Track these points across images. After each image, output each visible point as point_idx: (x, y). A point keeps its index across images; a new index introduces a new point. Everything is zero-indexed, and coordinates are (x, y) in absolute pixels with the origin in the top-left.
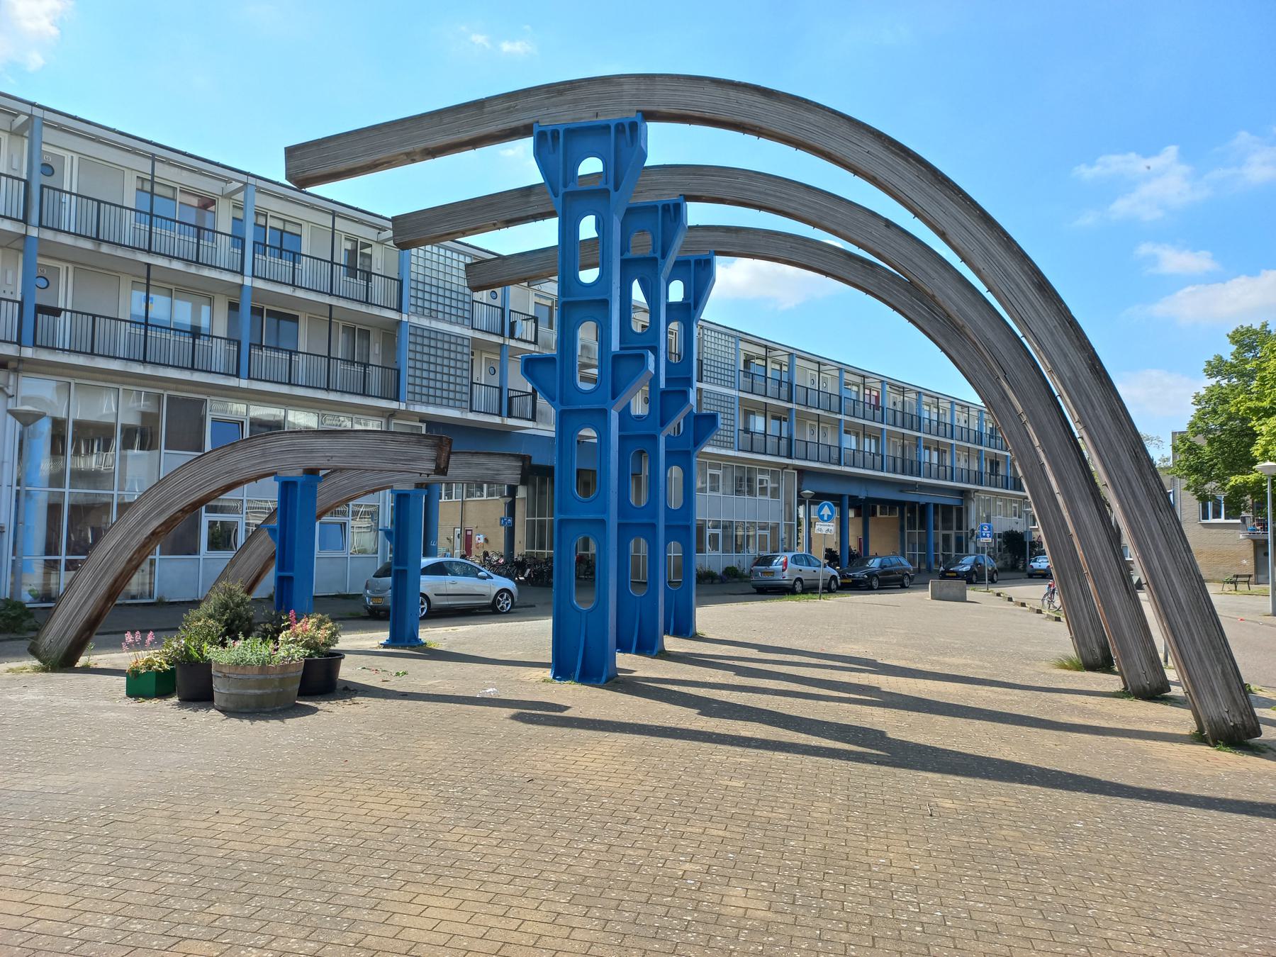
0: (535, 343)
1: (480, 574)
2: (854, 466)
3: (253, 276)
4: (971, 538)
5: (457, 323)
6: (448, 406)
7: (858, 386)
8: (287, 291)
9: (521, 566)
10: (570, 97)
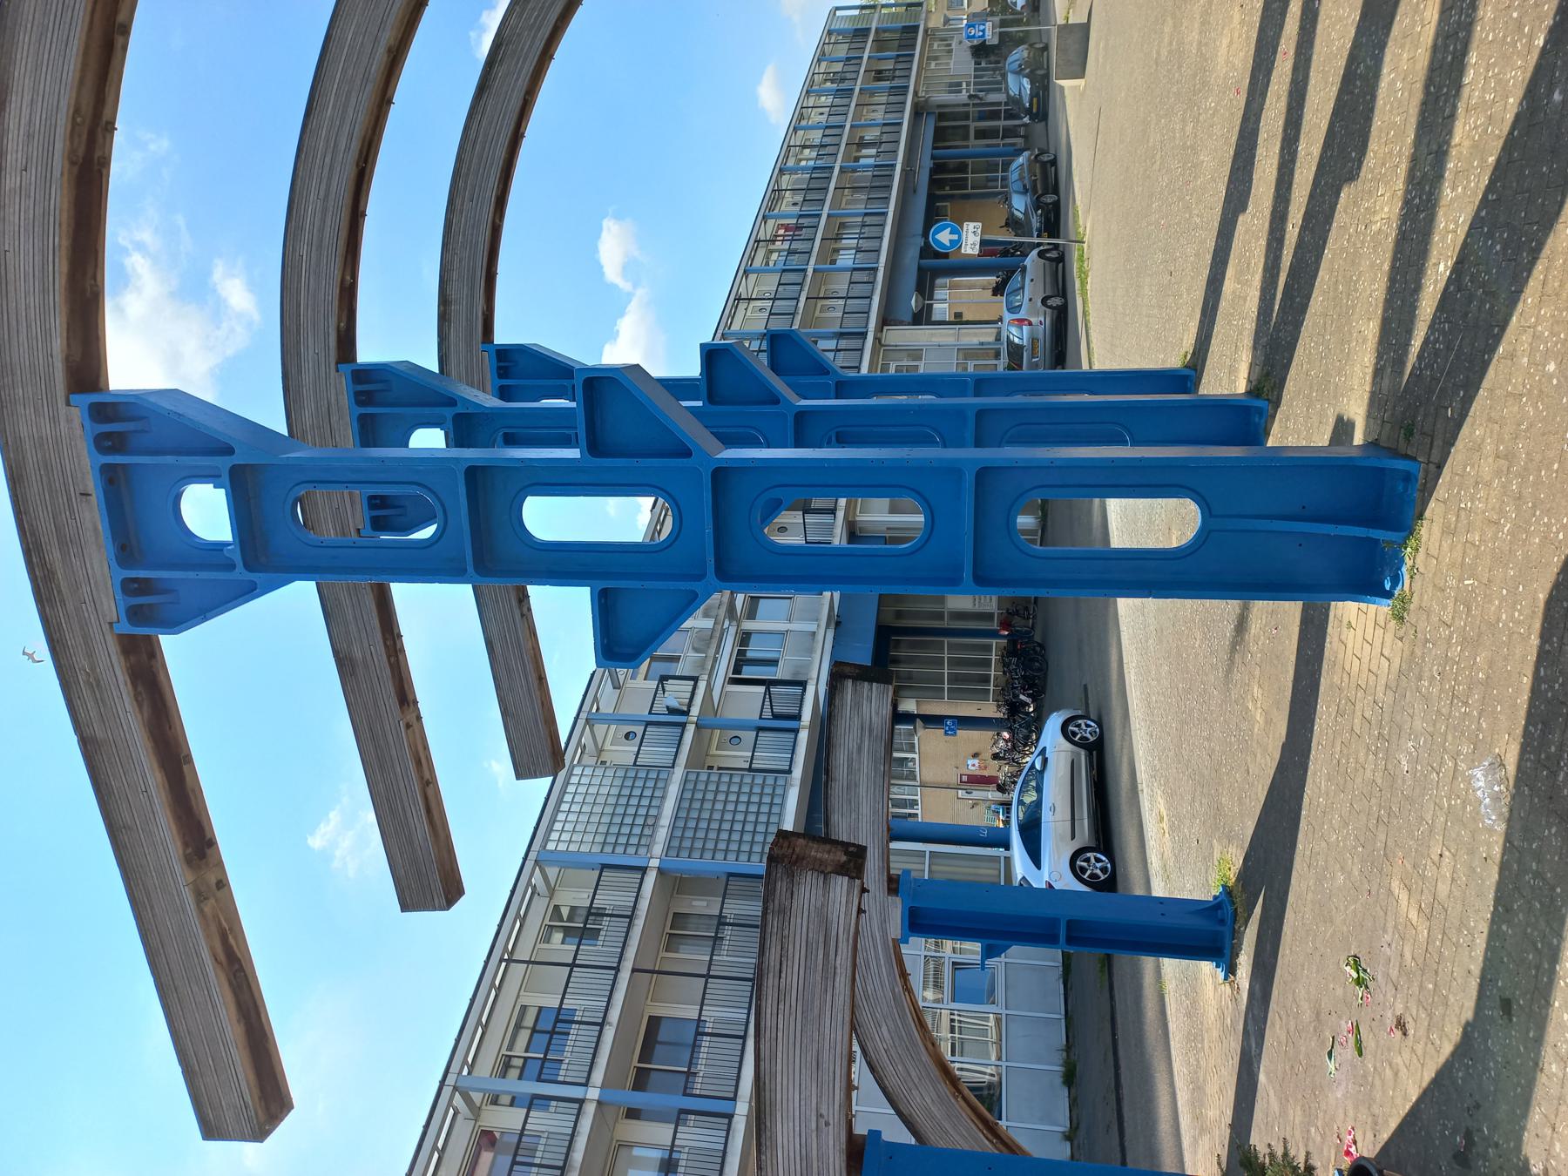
0: (695, 679)
1: (1038, 767)
3: (586, 1085)
4: (981, 99)
5: (665, 789)
6: (782, 805)
7: (771, 252)
8: (609, 1034)
9: (1014, 708)
10: (57, 554)
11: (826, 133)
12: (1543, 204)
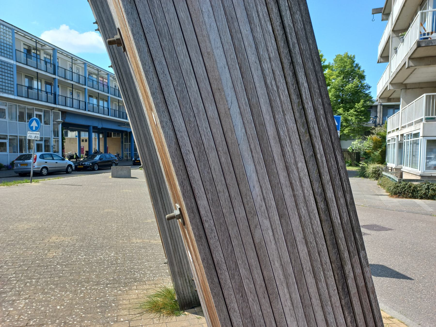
2: (93, 112)
11: (94, 82)
12: (98, 312)
